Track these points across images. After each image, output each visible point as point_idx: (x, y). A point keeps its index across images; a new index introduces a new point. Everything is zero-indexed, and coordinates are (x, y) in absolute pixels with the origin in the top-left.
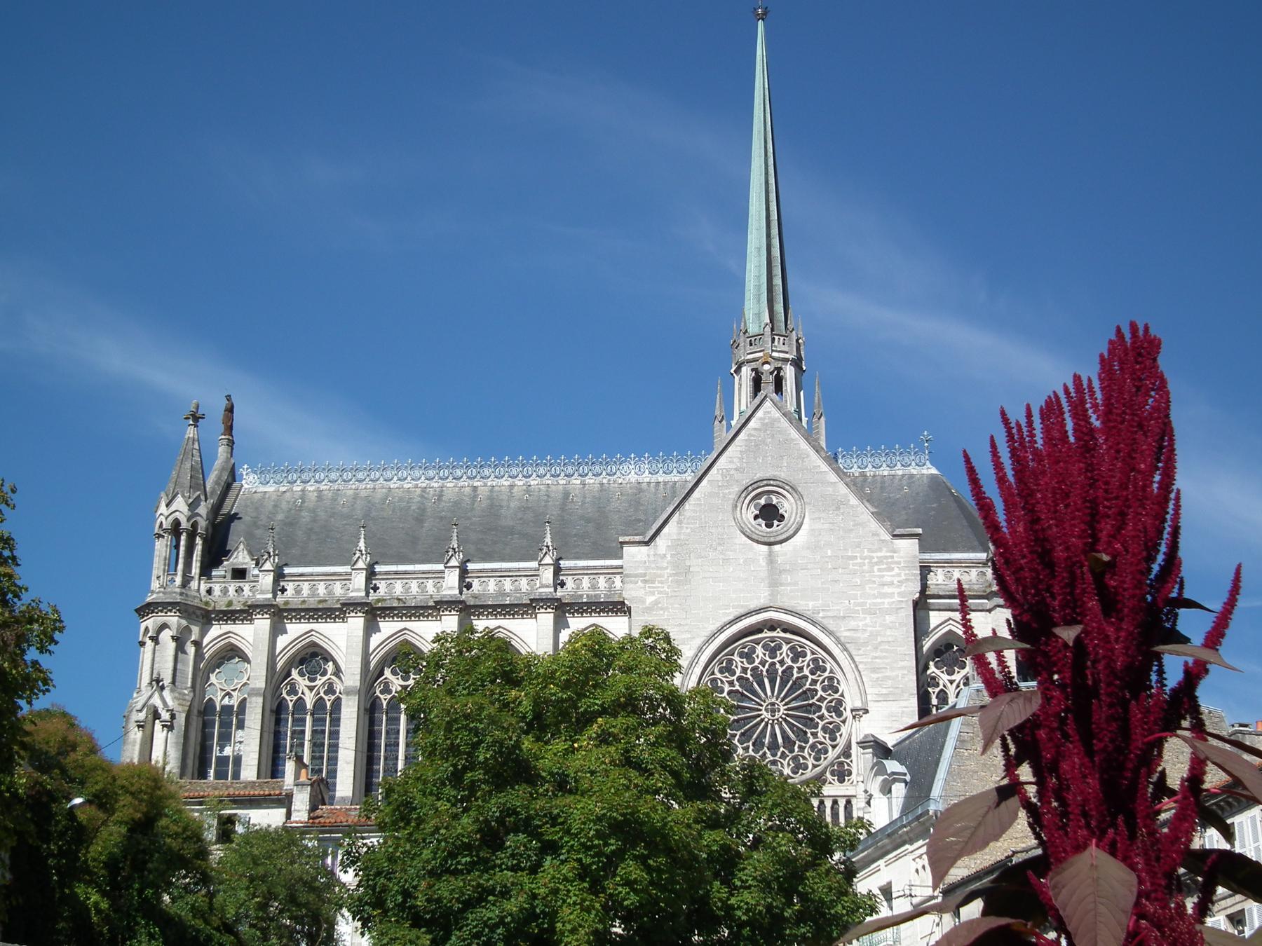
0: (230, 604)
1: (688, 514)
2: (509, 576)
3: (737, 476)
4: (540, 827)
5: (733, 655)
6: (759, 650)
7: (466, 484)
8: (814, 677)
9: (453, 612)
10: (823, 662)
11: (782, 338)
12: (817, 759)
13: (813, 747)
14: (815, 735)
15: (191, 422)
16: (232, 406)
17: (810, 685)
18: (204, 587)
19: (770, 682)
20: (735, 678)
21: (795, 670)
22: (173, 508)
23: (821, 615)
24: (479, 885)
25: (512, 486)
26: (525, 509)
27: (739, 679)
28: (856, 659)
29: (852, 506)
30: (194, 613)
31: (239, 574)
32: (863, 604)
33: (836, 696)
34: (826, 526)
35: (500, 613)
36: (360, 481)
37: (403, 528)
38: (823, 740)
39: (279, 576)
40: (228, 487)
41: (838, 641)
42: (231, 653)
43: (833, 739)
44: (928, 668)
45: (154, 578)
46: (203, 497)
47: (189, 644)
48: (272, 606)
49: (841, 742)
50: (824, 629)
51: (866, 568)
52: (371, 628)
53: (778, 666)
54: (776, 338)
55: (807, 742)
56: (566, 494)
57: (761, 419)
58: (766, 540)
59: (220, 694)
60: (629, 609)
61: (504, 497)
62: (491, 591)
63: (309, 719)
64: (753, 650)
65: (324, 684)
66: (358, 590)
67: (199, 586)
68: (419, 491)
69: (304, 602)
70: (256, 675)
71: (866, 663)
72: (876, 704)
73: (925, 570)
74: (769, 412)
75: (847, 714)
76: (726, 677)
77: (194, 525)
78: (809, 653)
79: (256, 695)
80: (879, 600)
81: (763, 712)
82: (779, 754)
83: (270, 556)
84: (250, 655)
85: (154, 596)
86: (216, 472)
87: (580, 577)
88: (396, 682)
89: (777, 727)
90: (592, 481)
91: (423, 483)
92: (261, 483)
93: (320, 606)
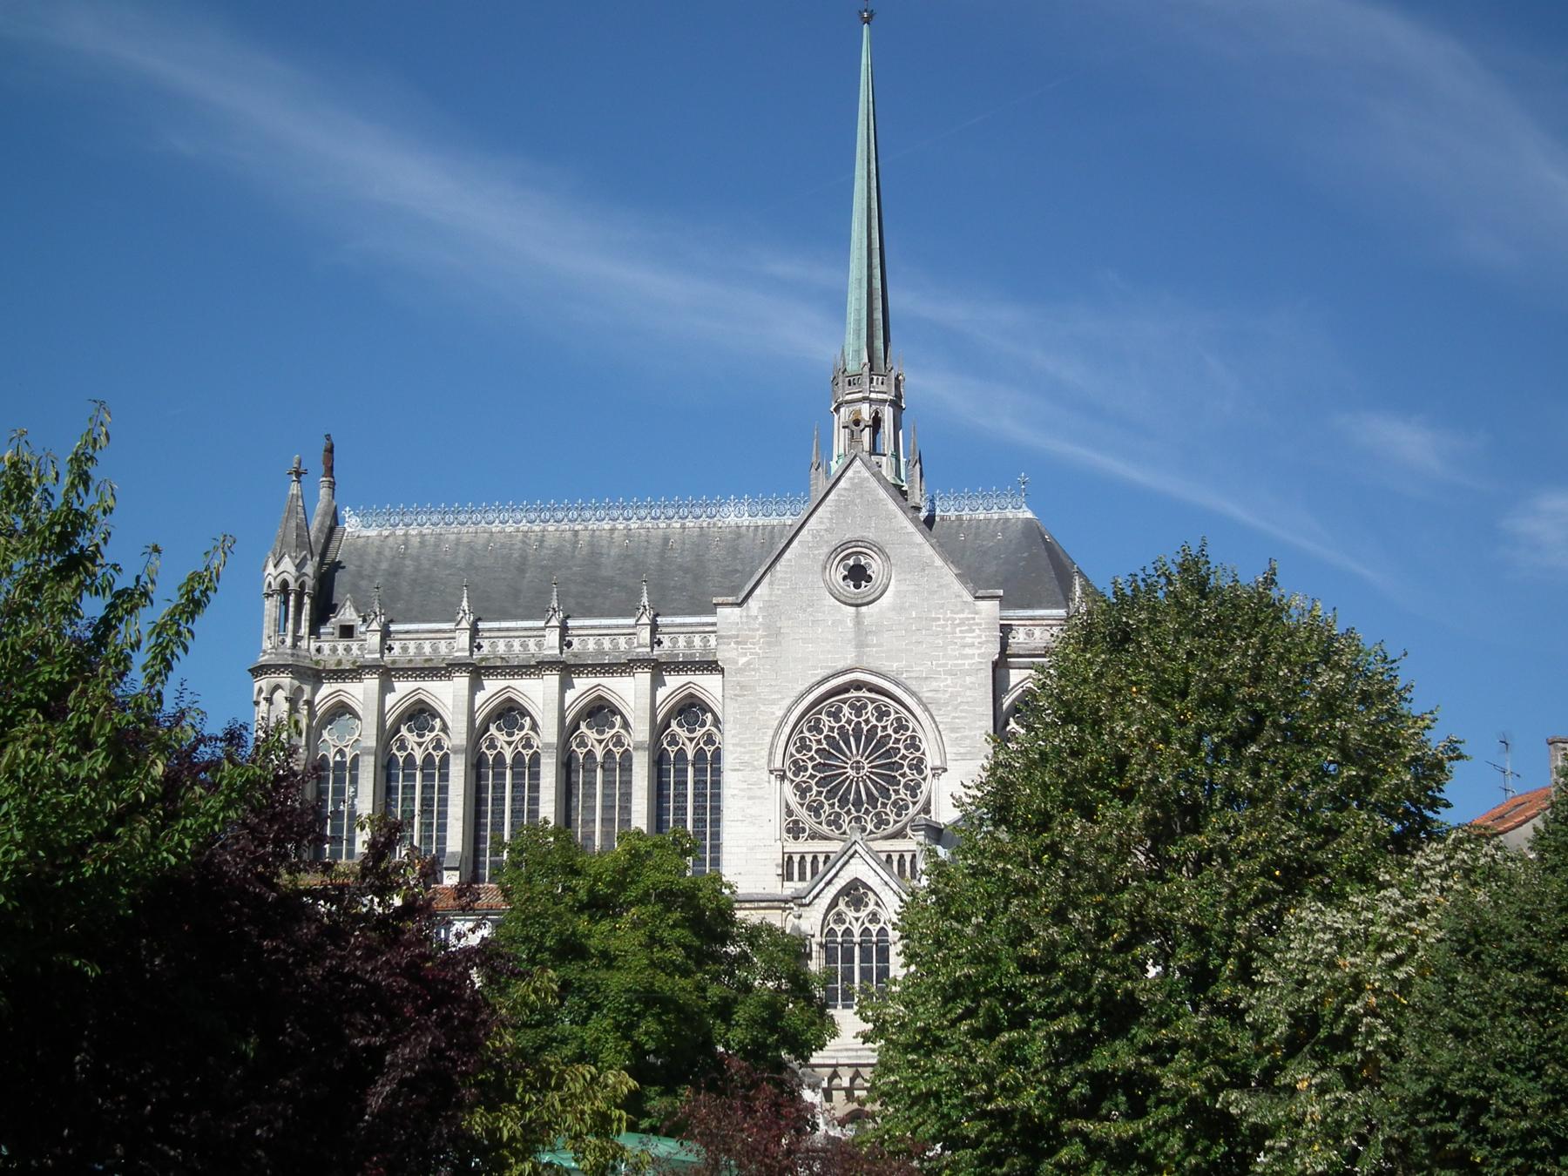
0: (339, 662)
1: (779, 575)
2: (607, 635)
3: (827, 536)
4: (588, 993)
5: (821, 714)
6: (846, 709)
7: (567, 527)
8: (897, 736)
9: (554, 672)
10: (906, 721)
11: (880, 378)
12: (899, 815)
13: (895, 803)
14: (896, 792)
15: (294, 478)
16: (332, 446)
17: (894, 743)
18: (313, 645)
19: (856, 740)
20: (822, 736)
21: (880, 729)
22: (281, 568)
23: (904, 676)
24: (546, 1036)
25: (612, 530)
26: (625, 557)
27: (827, 737)
28: (937, 719)
29: (937, 567)
30: (305, 673)
31: (347, 632)
32: (945, 665)
33: (918, 754)
34: (911, 588)
35: (600, 672)
36: (463, 524)
37: (504, 579)
38: (904, 797)
39: (386, 634)
40: (332, 530)
41: (920, 701)
42: (341, 710)
43: (914, 796)
44: (1009, 724)
45: (265, 637)
46: (309, 557)
47: (301, 703)
48: (380, 666)
49: (922, 799)
50: (907, 690)
51: (948, 629)
52: (475, 686)
53: (863, 725)
54: (875, 377)
55: (889, 799)
56: (666, 540)
57: (851, 478)
58: (853, 602)
59: (333, 751)
60: (723, 670)
61: (604, 543)
62: (591, 650)
63: (418, 775)
64: (840, 709)
65: (432, 740)
66: (463, 650)
67: (308, 645)
68: (520, 534)
69: (410, 661)
70: (366, 734)
71: (946, 723)
72: (955, 763)
73: (1006, 630)
74: (859, 472)
75: (928, 772)
76: (805, 755)
77: (302, 586)
78: (892, 712)
79: (368, 754)
80: (960, 662)
81: (849, 770)
82: (863, 810)
83: (376, 616)
84: (360, 713)
85: (266, 657)
86: (319, 518)
87: (676, 636)
88: (501, 737)
89: (861, 784)
90: (692, 524)
91: (524, 526)
92: (363, 526)
93: (426, 666)
